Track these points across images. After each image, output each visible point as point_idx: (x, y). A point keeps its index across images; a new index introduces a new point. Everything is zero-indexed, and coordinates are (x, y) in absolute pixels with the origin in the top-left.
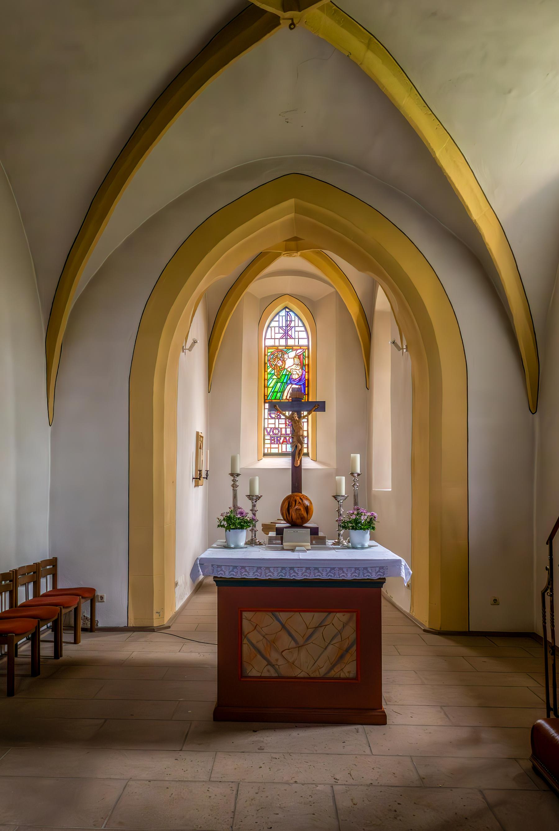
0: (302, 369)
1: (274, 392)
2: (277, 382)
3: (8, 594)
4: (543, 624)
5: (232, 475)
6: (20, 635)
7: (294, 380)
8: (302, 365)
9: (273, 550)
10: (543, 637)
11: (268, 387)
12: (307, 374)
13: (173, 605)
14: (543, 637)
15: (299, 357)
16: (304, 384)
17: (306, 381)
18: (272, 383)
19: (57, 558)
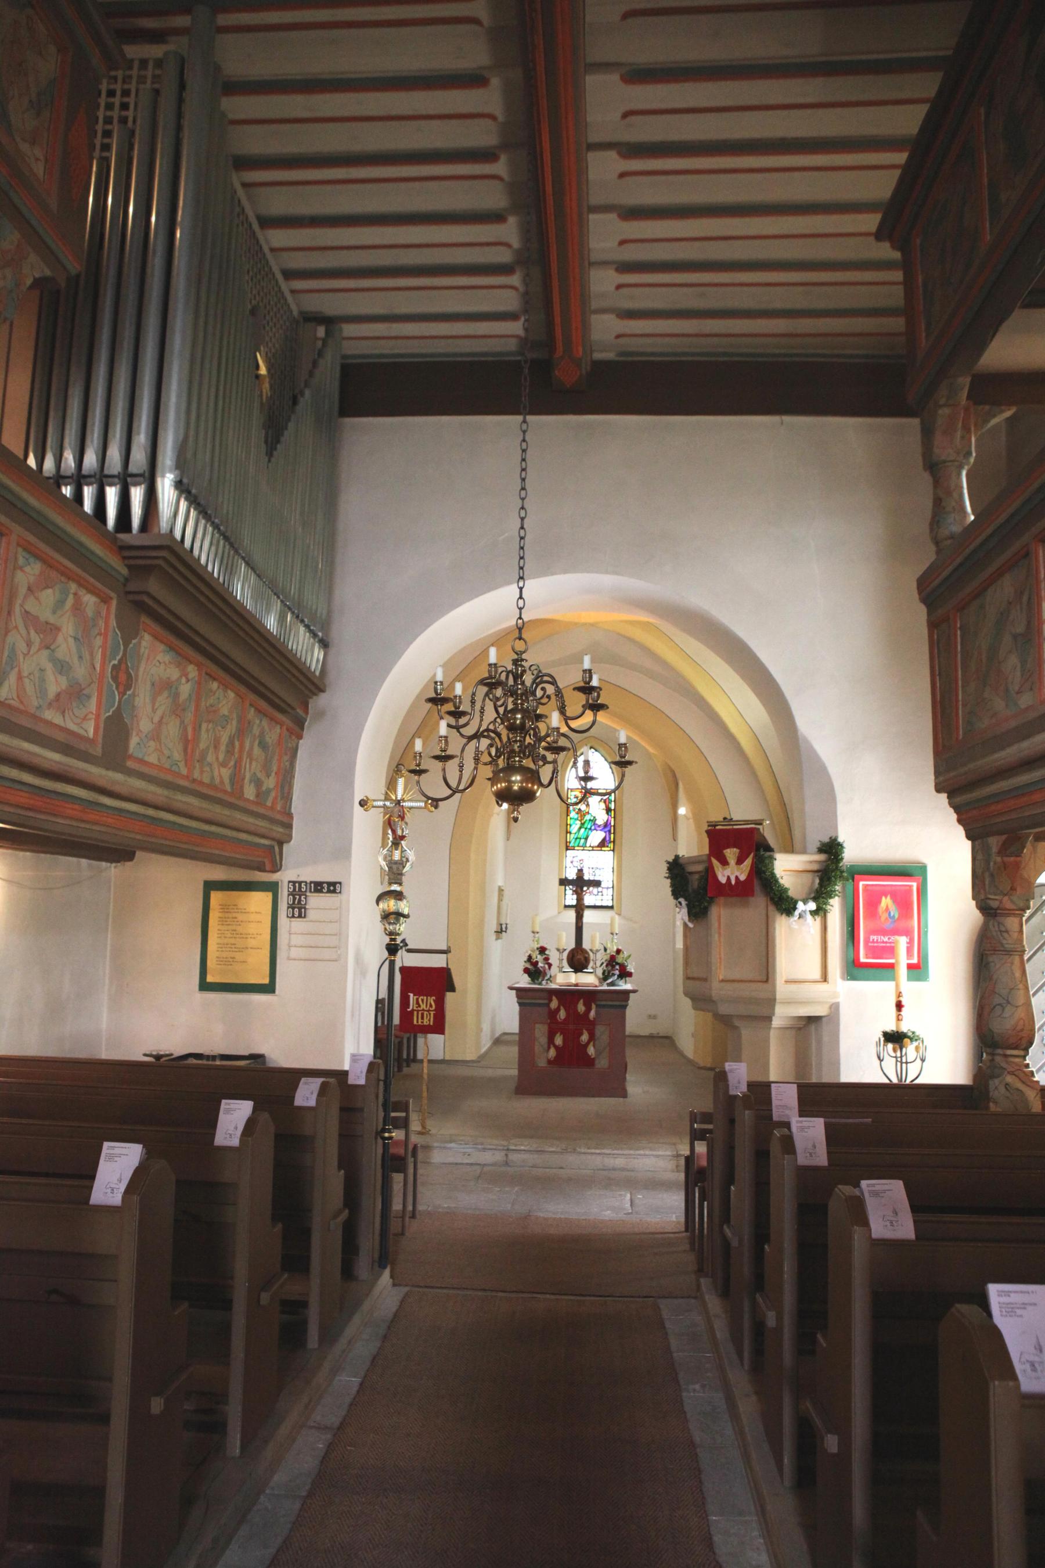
0: (608, 814)
1: (577, 838)
2: (580, 828)
3: (262, 1303)
4: (314, 657)
5: (533, 932)
6: (279, 812)
7: (599, 826)
8: (608, 810)
9: (374, 1147)
10: (321, 1080)
11: (570, 833)
12: (613, 819)
13: (71, 466)
14: (322, 1079)
15: (605, 802)
16: (610, 831)
17: (612, 828)
18: (574, 829)
19: (351, 1054)
